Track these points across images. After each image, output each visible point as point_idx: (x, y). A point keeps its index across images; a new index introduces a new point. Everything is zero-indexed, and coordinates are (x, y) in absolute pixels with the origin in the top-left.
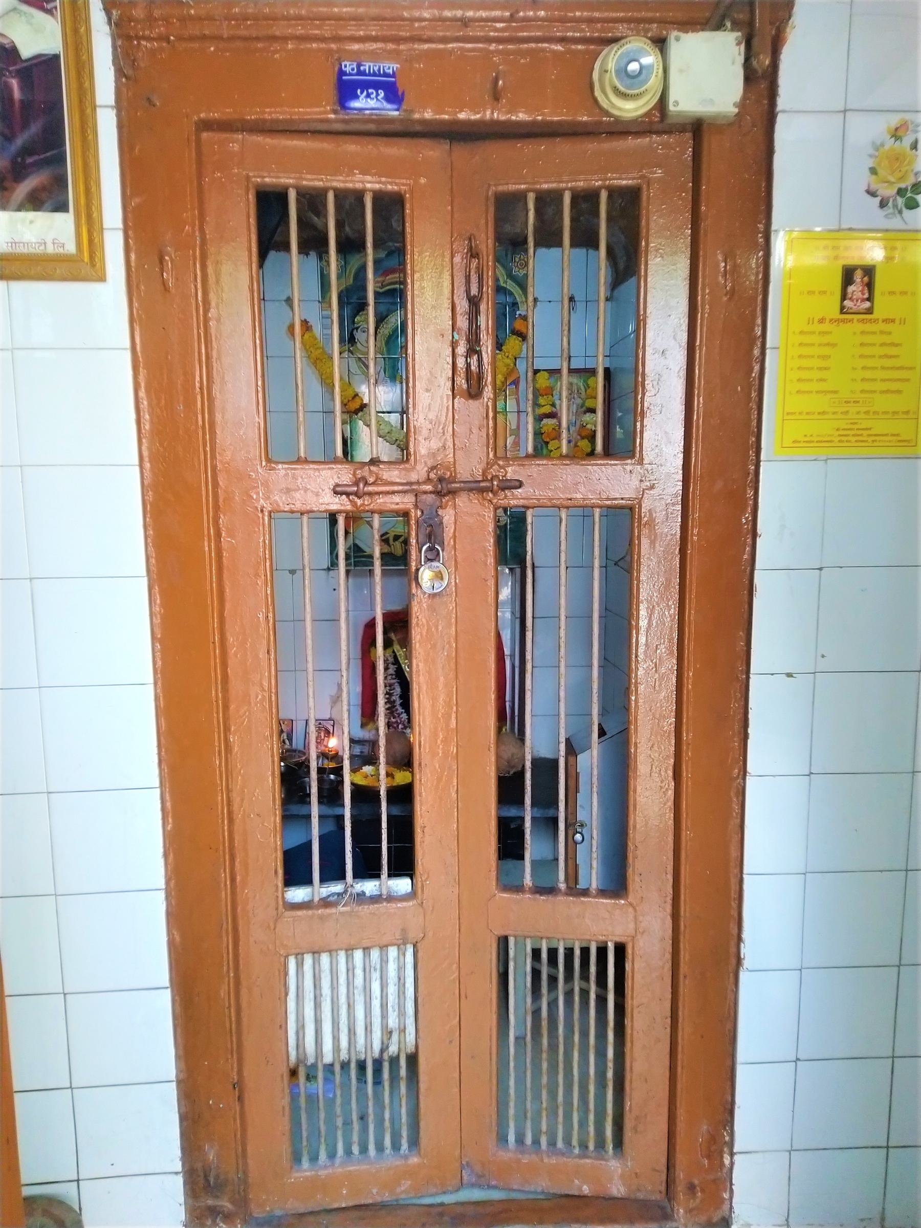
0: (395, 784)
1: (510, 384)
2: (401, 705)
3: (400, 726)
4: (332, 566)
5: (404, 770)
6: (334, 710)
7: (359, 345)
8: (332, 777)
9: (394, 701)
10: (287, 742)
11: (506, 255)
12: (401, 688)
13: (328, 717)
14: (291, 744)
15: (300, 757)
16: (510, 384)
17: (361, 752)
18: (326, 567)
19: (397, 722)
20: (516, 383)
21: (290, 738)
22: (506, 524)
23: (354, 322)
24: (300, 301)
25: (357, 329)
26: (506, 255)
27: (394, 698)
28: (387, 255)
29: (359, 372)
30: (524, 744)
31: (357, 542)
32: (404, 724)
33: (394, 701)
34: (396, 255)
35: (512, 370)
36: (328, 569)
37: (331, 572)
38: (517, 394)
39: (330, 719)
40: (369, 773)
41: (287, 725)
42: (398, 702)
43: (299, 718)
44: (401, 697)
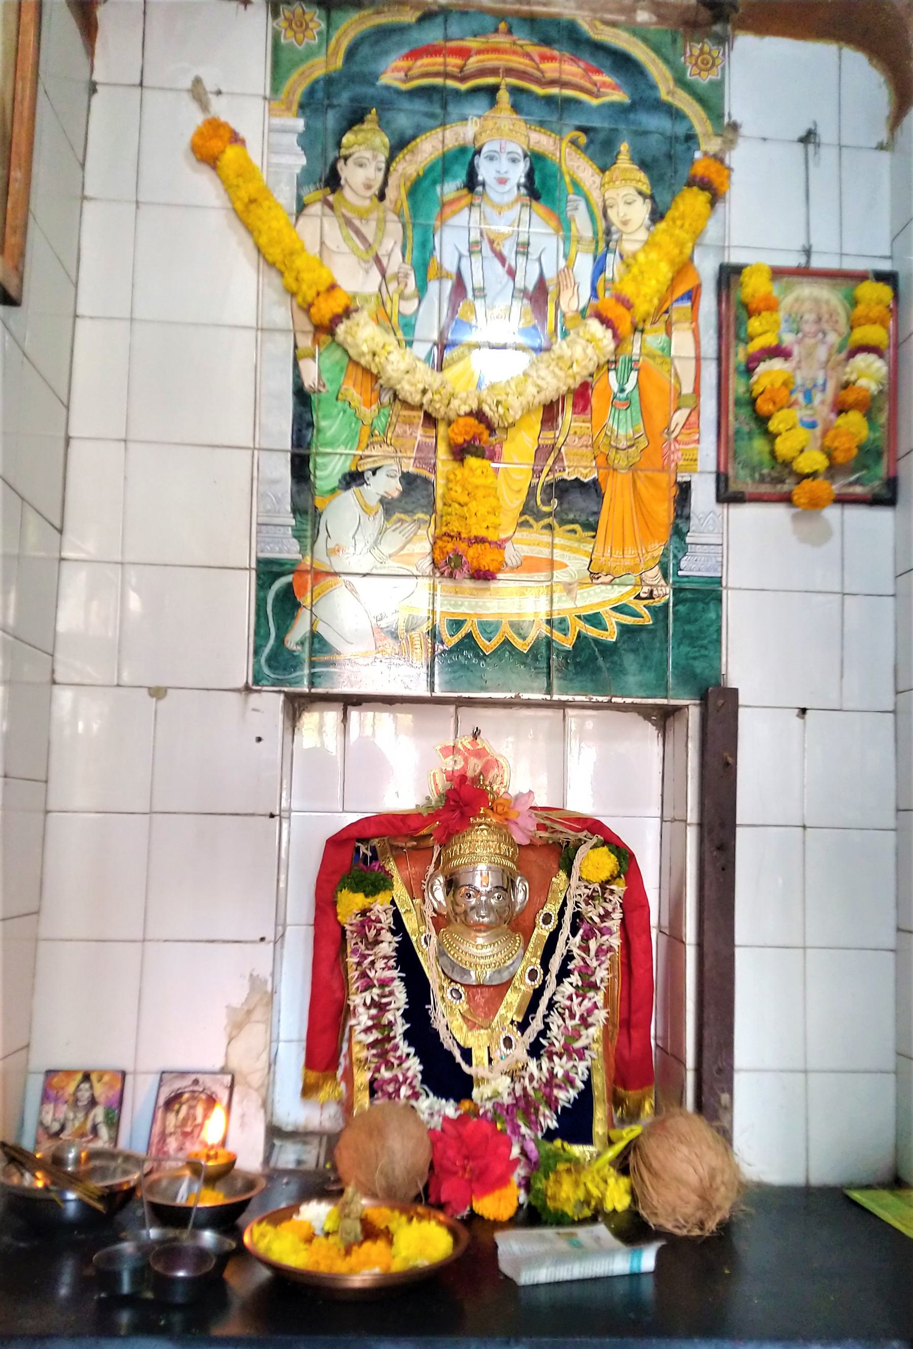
0: (397, 1266)
1: (682, 298)
2: (407, 1035)
3: (404, 1091)
4: (256, 681)
5: (421, 1218)
6: (239, 1046)
7: (347, 192)
8: (208, 1237)
9: (391, 1025)
10: (104, 1132)
11: (674, 41)
12: (409, 994)
13: (218, 1064)
14: (115, 1140)
15: (126, 1173)
16: (682, 298)
17: (299, 1162)
18: (241, 684)
19: (395, 1079)
20: (692, 296)
21: (114, 1122)
22: (666, 605)
23: (339, 145)
24: (258, 524)
25: (346, 159)
26: (674, 41)
27: (389, 1016)
28: (421, 20)
29: (344, 248)
30: (731, 1144)
31: (321, 629)
32: (412, 1086)
33: (391, 1025)
34: (440, 20)
35: (684, 268)
36: (247, 689)
37: (254, 697)
38: (695, 319)
39: (223, 1071)
40: (317, 1227)
41: (111, 1086)
42: (401, 1027)
43: (141, 1067)
44: (406, 1015)
